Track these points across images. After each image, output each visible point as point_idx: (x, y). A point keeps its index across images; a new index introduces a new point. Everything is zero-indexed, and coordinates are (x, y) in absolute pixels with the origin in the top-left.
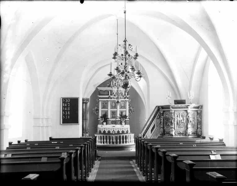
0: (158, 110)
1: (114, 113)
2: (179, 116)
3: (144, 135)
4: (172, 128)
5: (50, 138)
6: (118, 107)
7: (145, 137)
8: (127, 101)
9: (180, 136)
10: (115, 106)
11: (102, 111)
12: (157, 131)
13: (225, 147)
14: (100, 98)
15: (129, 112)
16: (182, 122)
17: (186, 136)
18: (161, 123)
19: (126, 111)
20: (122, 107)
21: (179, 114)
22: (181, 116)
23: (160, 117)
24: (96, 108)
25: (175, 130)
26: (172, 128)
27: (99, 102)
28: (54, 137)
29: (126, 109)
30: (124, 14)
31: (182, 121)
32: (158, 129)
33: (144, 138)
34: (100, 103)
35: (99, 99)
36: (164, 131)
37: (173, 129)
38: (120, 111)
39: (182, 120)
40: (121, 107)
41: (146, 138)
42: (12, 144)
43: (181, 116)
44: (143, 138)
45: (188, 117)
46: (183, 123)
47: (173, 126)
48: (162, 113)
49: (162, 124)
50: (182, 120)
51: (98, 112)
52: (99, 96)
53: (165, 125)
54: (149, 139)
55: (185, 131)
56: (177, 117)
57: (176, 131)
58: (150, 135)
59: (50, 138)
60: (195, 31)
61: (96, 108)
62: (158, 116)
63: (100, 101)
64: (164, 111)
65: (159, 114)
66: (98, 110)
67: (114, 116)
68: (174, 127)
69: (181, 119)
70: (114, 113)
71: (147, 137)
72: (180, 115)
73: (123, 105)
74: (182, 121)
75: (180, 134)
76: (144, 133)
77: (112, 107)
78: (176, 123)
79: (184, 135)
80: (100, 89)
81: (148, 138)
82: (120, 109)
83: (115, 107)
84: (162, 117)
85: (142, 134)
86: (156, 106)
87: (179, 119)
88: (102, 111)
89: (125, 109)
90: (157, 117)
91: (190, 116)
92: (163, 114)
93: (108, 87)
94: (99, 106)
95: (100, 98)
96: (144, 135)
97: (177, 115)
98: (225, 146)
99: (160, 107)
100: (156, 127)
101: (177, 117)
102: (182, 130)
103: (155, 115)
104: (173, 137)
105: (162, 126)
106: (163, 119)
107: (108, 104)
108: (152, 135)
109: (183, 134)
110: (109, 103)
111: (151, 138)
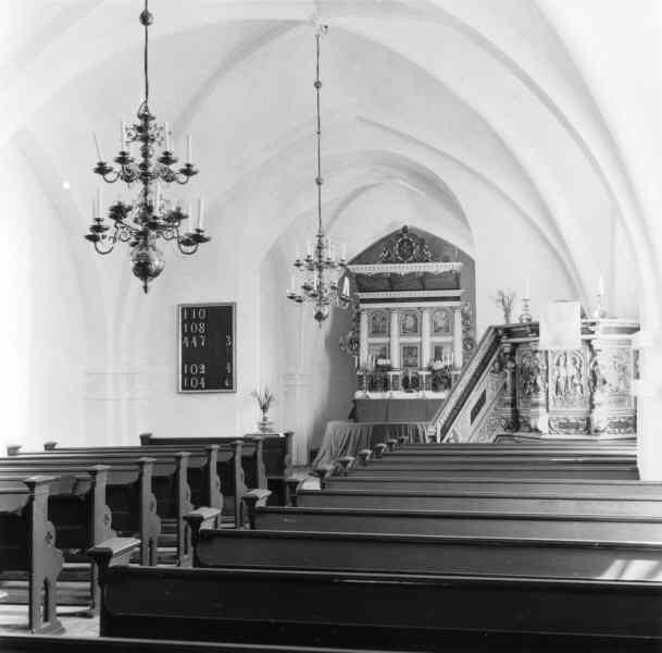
0: (497, 342)
1: (410, 351)
2: (562, 363)
3: (445, 430)
4: (536, 405)
5: (146, 439)
6: (427, 327)
7: (449, 435)
8: (456, 308)
9: (567, 433)
10: (416, 326)
11: (370, 345)
12: (493, 415)
13: (635, 482)
14: (364, 301)
15: (465, 347)
16: (575, 385)
17: (589, 433)
18: (505, 386)
19: (452, 344)
20: (440, 328)
21: (565, 354)
22: (569, 362)
23: (502, 366)
24: (350, 334)
25: (548, 410)
26: (536, 405)
27: (359, 314)
28: (156, 435)
29: (421, 335)
30: (143, 27)
31: (576, 381)
32: (495, 409)
33: (444, 441)
34: (364, 319)
35: (362, 306)
36: (516, 413)
37: (542, 410)
38: (433, 343)
39: (573, 377)
40: (436, 331)
41: (452, 441)
42: (57, 447)
43: (569, 362)
44: (441, 440)
45: (596, 364)
46: (578, 388)
47: (542, 398)
48: (507, 350)
49: (509, 389)
50: (573, 377)
51: (358, 349)
52: (359, 294)
53: (519, 394)
54: (462, 445)
55: (583, 416)
56: (558, 364)
57: (554, 417)
58: (469, 428)
59: (146, 439)
60: (486, 36)
61: (350, 334)
62: (497, 365)
63: (363, 310)
64: (516, 345)
65: (499, 356)
66: (358, 342)
67: (411, 361)
68: (544, 402)
69: (572, 371)
70: (410, 351)
71: (455, 435)
72: (568, 359)
73: (441, 323)
74: (576, 381)
75: (566, 426)
76: (446, 422)
77: (405, 331)
78: (554, 386)
79: (581, 429)
80: (357, 272)
81: (462, 440)
82: (431, 335)
83: (416, 330)
84: (510, 365)
85: (439, 427)
86: (490, 328)
87: (563, 374)
88: (370, 345)
89: (388, 339)
90: (493, 365)
91: (599, 362)
92: (513, 353)
93: (384, 262)
94: (358, 326)
95: (364, 301)
96: (445, 430)
97: (556, 358)
98: (638, 478)
99: (500, 332)
100: (488, 401)
101: (558, 364)
102: (575, 412)
103: (485, 357)
104: (543, 437)
105: (508, 398)
106: (514, 374)
107: (390, 318)
108: (475, 430)
109: (577, 426)
110: (395, 318)
111: (471, 441)
